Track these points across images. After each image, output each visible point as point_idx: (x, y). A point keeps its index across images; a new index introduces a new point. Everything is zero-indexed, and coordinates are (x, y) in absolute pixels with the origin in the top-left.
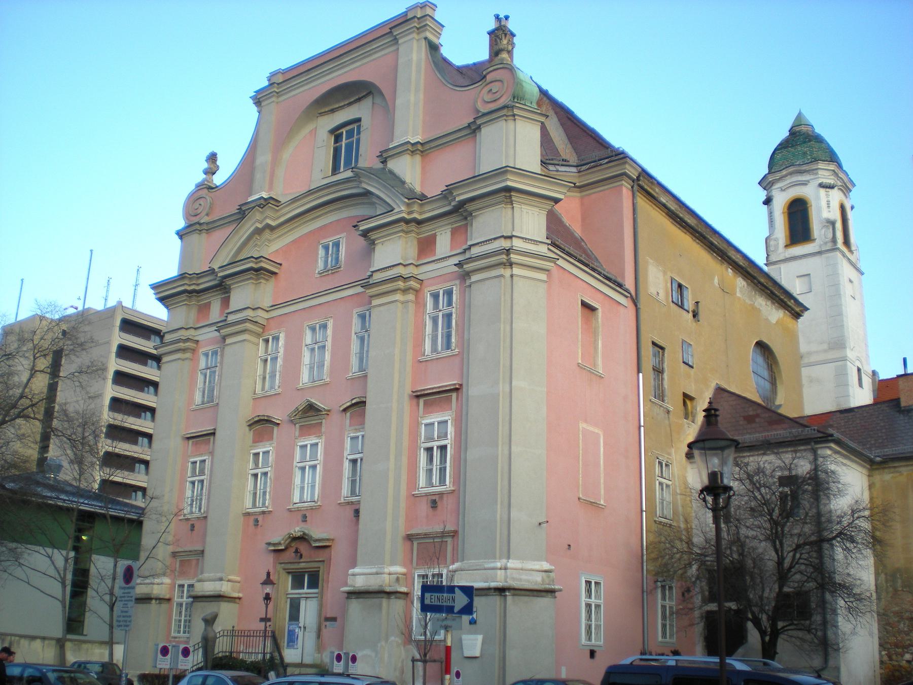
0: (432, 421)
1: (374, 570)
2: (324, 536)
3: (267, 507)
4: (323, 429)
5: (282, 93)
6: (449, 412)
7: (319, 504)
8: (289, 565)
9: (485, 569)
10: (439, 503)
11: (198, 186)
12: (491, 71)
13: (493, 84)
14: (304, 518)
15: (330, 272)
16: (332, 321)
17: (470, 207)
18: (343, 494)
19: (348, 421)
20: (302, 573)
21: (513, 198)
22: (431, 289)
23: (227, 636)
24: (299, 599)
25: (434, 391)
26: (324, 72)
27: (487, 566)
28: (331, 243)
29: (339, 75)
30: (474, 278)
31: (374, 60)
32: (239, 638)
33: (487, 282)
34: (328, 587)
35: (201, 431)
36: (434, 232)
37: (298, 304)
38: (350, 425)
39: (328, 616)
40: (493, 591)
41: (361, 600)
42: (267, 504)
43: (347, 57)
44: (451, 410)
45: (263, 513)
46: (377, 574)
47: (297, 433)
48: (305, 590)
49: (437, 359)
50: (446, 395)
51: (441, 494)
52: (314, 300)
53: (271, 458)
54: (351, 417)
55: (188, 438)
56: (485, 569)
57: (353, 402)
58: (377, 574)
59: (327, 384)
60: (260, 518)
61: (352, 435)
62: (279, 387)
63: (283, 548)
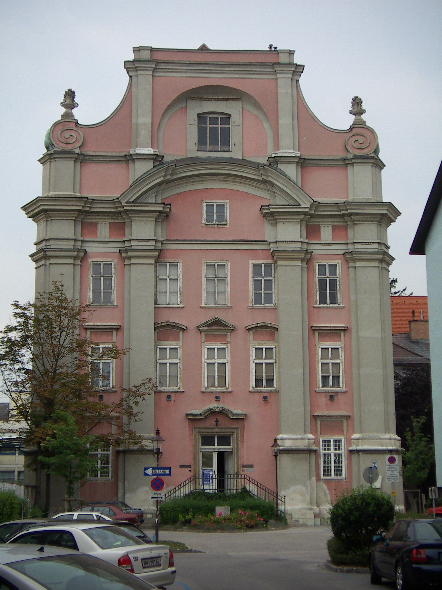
0: (327, 347)
1: (300, 437)
2: (239, 411)
3: (179, 388)
4: (229, 339)
5: (160, 70)
6: (340, 343)
7: (230, 390)
8: (204, 429)
9: (380, 439)
10: (335, 398)
11: (62, 116)
12: (357, 127)
13: (361, 137)
14: (217, 398)
15: (216, 226)
16: (229, 264)
17: (277, 216)
18: (251, 385)
19: (251, 337)
20: (229, 435)
21: (132, 219)
22: (95, 260)
23: (215, 479)
24: (212, 452)
25: (330, 328)
26: (166, 69)
27: (382, 437)
28: (215, 205)
29: (218, 78)
30: (133, 261)
31: (251, 78)
32: (243, 480)
33: (368, 268)
34: (243, 445)
35: (106, 325)
36: (319, 224)
37: (252, 245)
38: (253, 340)
39: (245, 464)
40: (387, 452)
41: (291, 455)
42: (179, 386)
43: (228, 67)
44: (340, 341)
45: (176, 392)
46: (302, 439)
47: (203, 339)
48: (216, 447)
49: (327, 308)
50: (330, 332)
51: (337, 393)
52: (199, 245)
53: (180, 352)
54: (254, 334)
55: (249, 330)
56: (380, 439)
57: (259, 325)
58: (302, 439)
59: (228, 308)
60: (173, 395)
61: (257, 347)
62: (181, 303)
63: (203, 418)
